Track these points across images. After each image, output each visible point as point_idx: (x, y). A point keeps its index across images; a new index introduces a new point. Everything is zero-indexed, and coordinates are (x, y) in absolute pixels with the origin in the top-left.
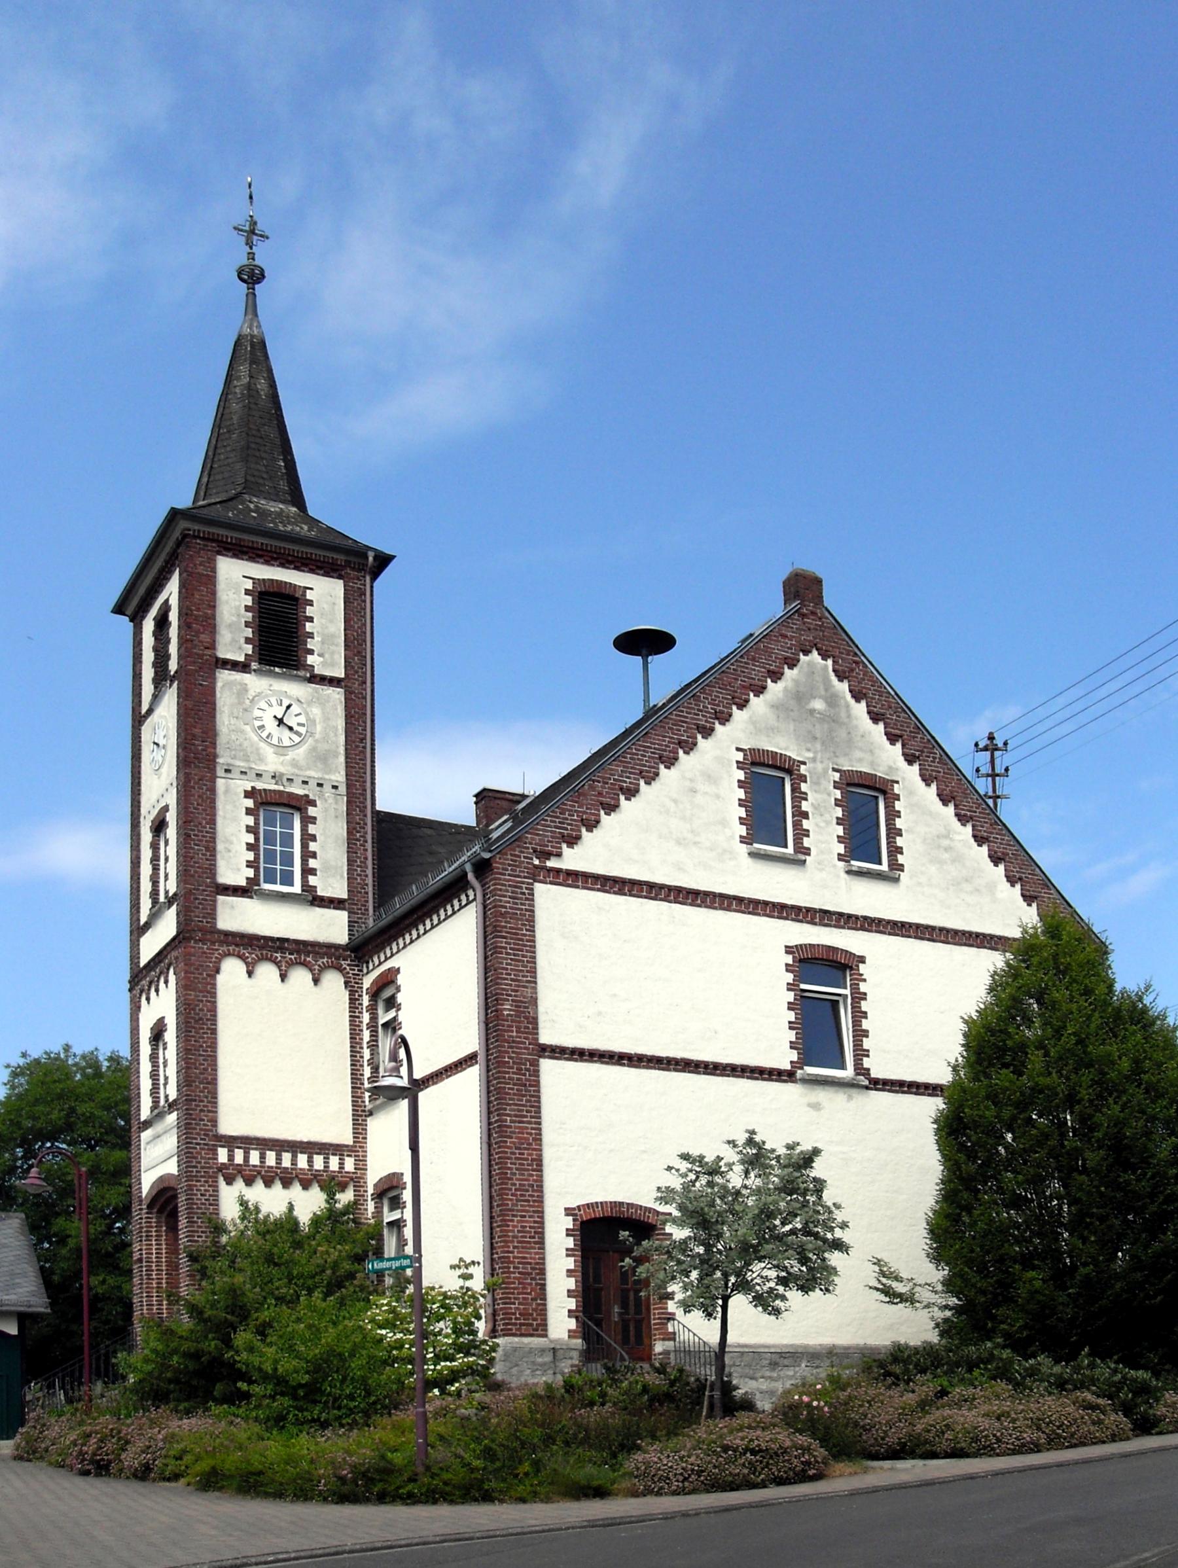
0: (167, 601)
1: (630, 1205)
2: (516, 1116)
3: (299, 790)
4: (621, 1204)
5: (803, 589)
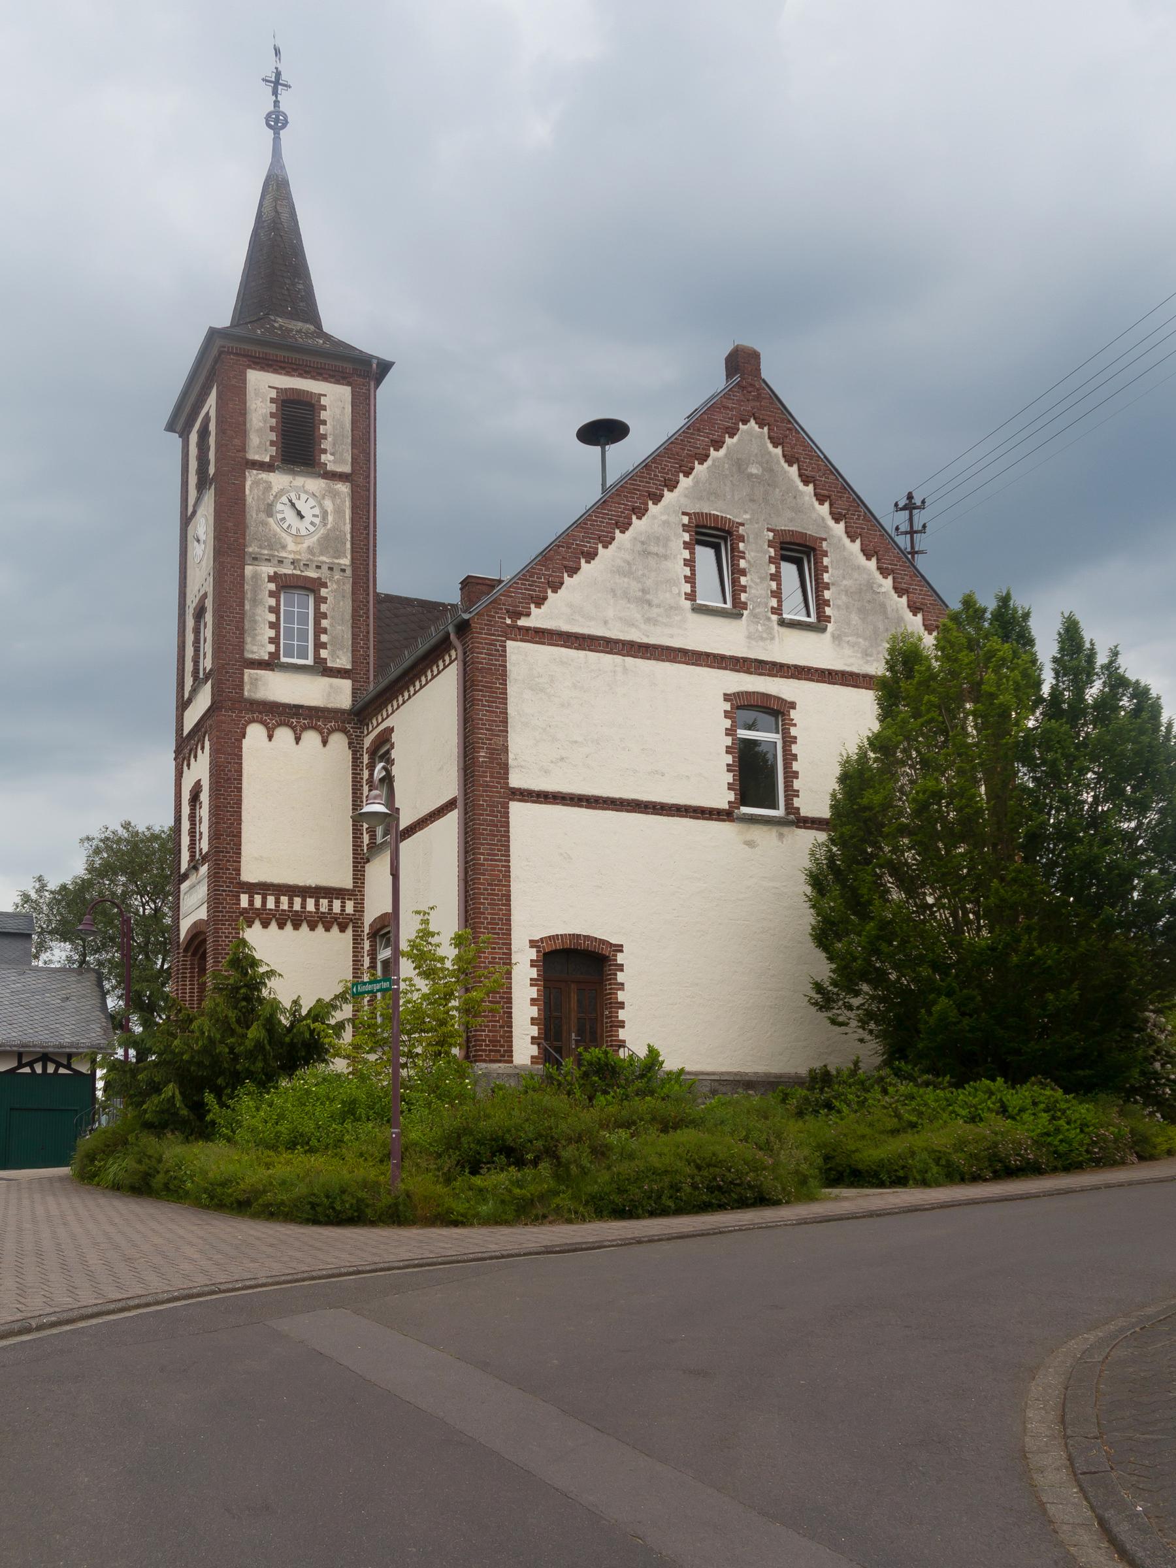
0: (208, 413)
1: (587, 937)
2: (489, 854)
3: (312, 574)
4: (579, 936)
5: (742, 363)
